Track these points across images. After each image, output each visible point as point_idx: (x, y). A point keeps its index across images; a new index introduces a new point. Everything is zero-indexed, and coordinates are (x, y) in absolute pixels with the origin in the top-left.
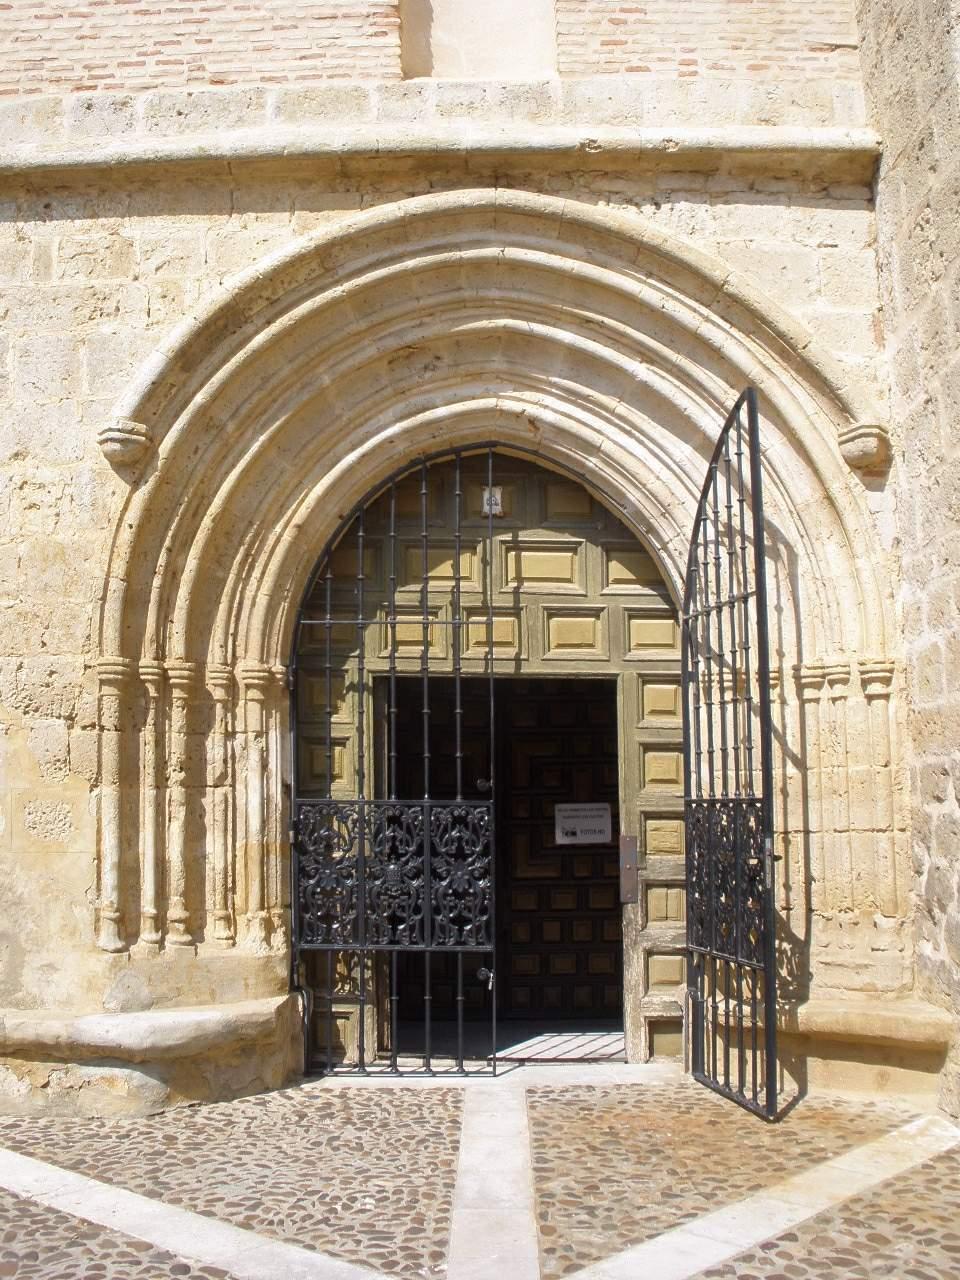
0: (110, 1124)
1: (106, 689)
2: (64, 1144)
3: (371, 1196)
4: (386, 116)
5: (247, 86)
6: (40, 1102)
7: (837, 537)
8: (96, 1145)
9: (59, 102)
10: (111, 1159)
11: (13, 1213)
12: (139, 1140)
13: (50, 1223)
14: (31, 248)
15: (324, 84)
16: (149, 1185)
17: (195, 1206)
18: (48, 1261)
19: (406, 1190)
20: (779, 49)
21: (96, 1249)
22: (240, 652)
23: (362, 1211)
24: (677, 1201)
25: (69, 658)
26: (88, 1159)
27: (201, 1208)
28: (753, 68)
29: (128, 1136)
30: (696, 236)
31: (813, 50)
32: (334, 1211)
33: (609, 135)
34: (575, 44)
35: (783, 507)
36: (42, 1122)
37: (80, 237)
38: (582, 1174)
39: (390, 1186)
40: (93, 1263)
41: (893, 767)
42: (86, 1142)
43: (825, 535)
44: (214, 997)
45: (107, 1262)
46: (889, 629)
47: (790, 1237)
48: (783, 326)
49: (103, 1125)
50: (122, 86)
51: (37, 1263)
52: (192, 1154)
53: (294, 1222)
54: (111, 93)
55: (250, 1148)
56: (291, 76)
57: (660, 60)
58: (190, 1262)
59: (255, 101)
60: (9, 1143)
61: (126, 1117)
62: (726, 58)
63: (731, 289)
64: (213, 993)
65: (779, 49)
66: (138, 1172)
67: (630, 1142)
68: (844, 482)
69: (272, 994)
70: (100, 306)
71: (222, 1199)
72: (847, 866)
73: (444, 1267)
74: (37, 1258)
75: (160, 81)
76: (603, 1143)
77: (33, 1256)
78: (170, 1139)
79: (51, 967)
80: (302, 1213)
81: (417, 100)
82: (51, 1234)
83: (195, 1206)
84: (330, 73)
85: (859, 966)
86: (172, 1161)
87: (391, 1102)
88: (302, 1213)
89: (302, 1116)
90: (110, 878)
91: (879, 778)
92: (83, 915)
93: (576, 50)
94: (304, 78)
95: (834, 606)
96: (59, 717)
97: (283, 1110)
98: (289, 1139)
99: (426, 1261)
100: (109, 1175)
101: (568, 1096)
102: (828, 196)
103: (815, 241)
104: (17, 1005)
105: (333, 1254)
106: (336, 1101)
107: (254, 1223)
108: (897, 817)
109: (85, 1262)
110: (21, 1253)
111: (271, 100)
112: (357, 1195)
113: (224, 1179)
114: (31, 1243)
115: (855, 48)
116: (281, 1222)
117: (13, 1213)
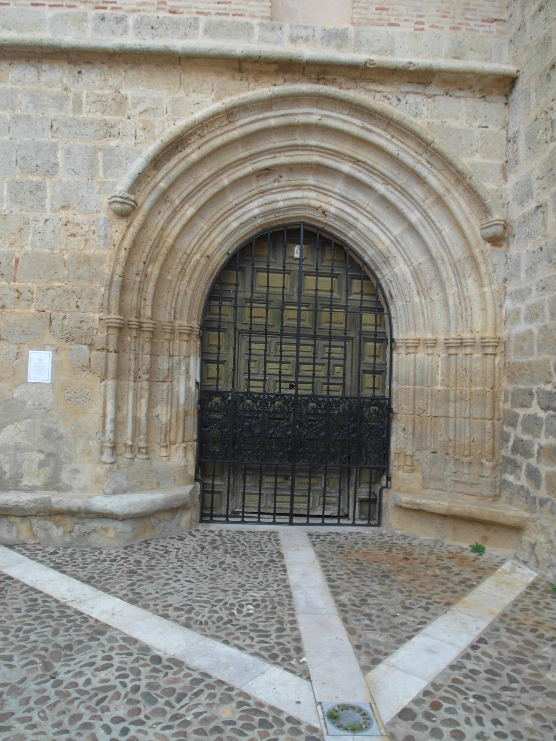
0: (105, 552)
1: (111, 331)
2: (82, 565)
3: (251, 604)
4: (262, 40)
5: (189, 16)
6: (68, 539)
7: (473, 276)
8: (99, 566)
9: (85, 14)
10: (107, 577)
11: (56, 614)
12: (121, 563)
13: (78, 622)
14: (71, 95)
15: (230, 19)
16: (131, 596)
17: (157, 610)
18: (79, 651)
19: (267, 599)
20: (466, 19)
21: (105, 643)
22: (178, 316)
23: (249, 615)
24: (411, 612)
25: (91, 314)
26: (95, 576)
27: (161, 612)
28: (453, 28)
29: (115, 560)
30: (418, 118)
31: (483, 21)
32: (232, 614)
33: (379, 59)
34: (362, 8)
35: (446, 259)
36: (70, 551)
37: (98, 92)
38: (355, 590)
39: (258, 596)
40: (105, 654)
41: (496, 389)
42: (93, 564)
43: (467, 273)
44: (158, 486)
45: (113, 654)
46: (498, 322)
47: (481, 640)
48: (460, 167)
49: (101, 553)
50: (121, 9)
51: (72, 653)
52: (151, 573)
53: (214, 623)
54: (115, 12)
55: (180, 569)
56: (213, 12)
57: (406, 20)
58: (161, 654)
59: (193, 24)
60: (52, 564)
61: (114, 548)
62: (439, 22)
63: (436, 146)
64: (158, 484)
65: (466, 19)
66: (124, 585)
67: (370, 569)
68: (481, 248)
69: (187, 484)
70: (109, 130)
71: (170, 605)
72: (468, 435)
73: (304, 659)
74: (71, 649)
75: (141, 8)
76: (357, 569)
77: (69, 647)
78: (138, 562)
79: (77, 471)
80: (216, 615)
81: (279, 32)
82: (79, 630)
83: (157, 610)
84: (234, 12)
85: (473, 484)
86: (140, 577)
87: (244, 539)
88: (216, 615)
89: (203, 548)
90: (109, 427)
91: (488, 394)
92: (94, 445)
93: (363, 11)
94: (220, 14)
95: (469, 309)
96: (85, 344)
97: (193, 544)
98: (199, 563)
99: (292, 653)
100: (108, 587)
101: (329, 538)
102: (485, 100)
103: (477, 124)
104: (58, 489)
105: (241, 648)
106: (217, 538)
107: (191, 622)
108: (497, 414)
109: (100, 655)
110: (63, 644)
111: (202, 25)
112: (244, 603)
113: (170, 591)
114: (68, 637)
115: (505, 21)
116: (206, 623)
117: (56, 614)
